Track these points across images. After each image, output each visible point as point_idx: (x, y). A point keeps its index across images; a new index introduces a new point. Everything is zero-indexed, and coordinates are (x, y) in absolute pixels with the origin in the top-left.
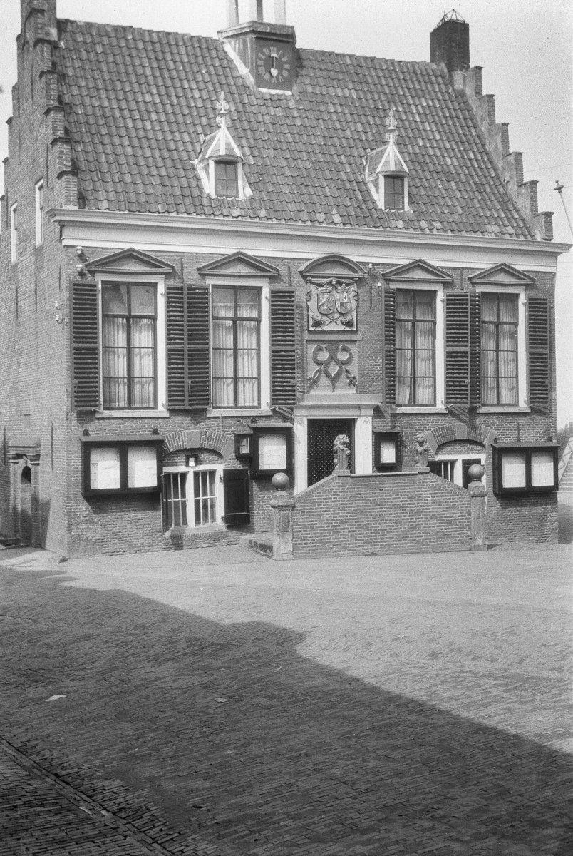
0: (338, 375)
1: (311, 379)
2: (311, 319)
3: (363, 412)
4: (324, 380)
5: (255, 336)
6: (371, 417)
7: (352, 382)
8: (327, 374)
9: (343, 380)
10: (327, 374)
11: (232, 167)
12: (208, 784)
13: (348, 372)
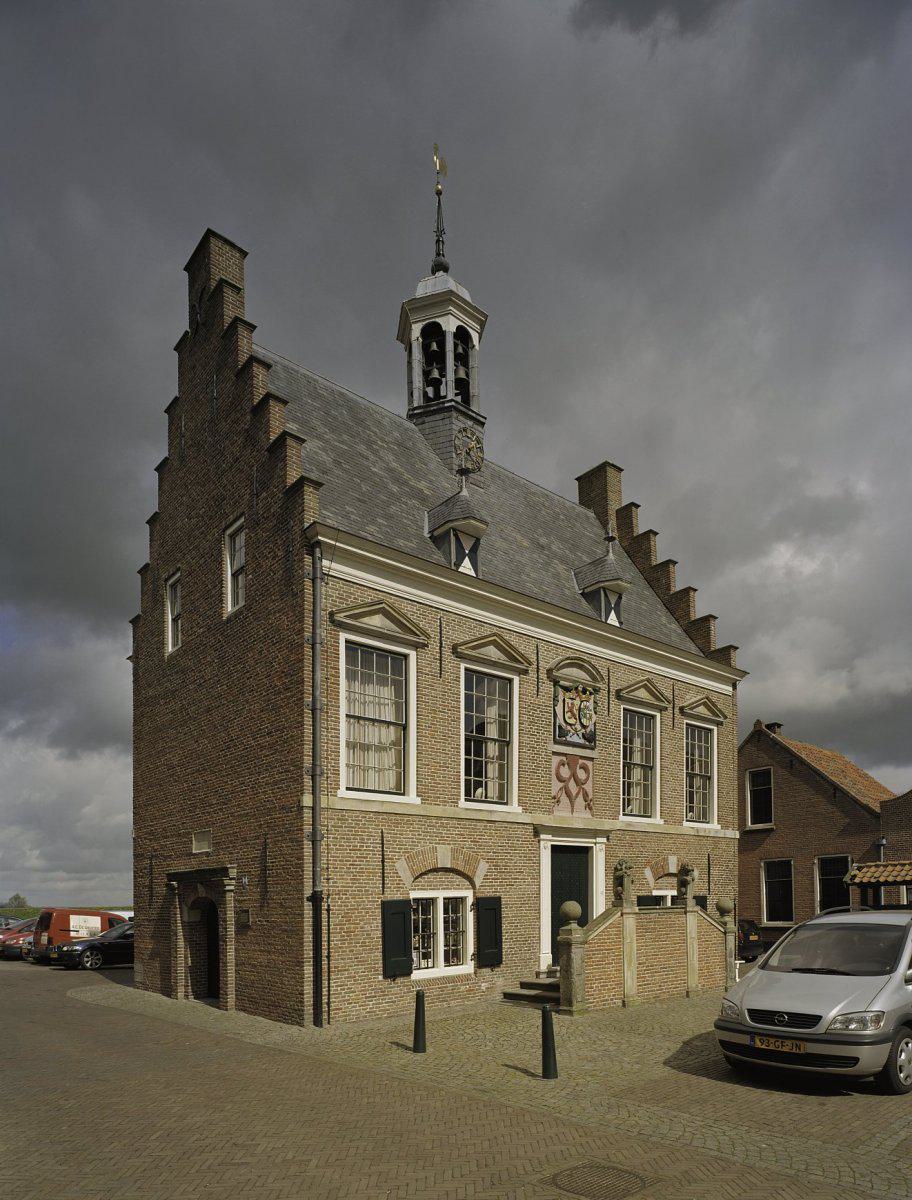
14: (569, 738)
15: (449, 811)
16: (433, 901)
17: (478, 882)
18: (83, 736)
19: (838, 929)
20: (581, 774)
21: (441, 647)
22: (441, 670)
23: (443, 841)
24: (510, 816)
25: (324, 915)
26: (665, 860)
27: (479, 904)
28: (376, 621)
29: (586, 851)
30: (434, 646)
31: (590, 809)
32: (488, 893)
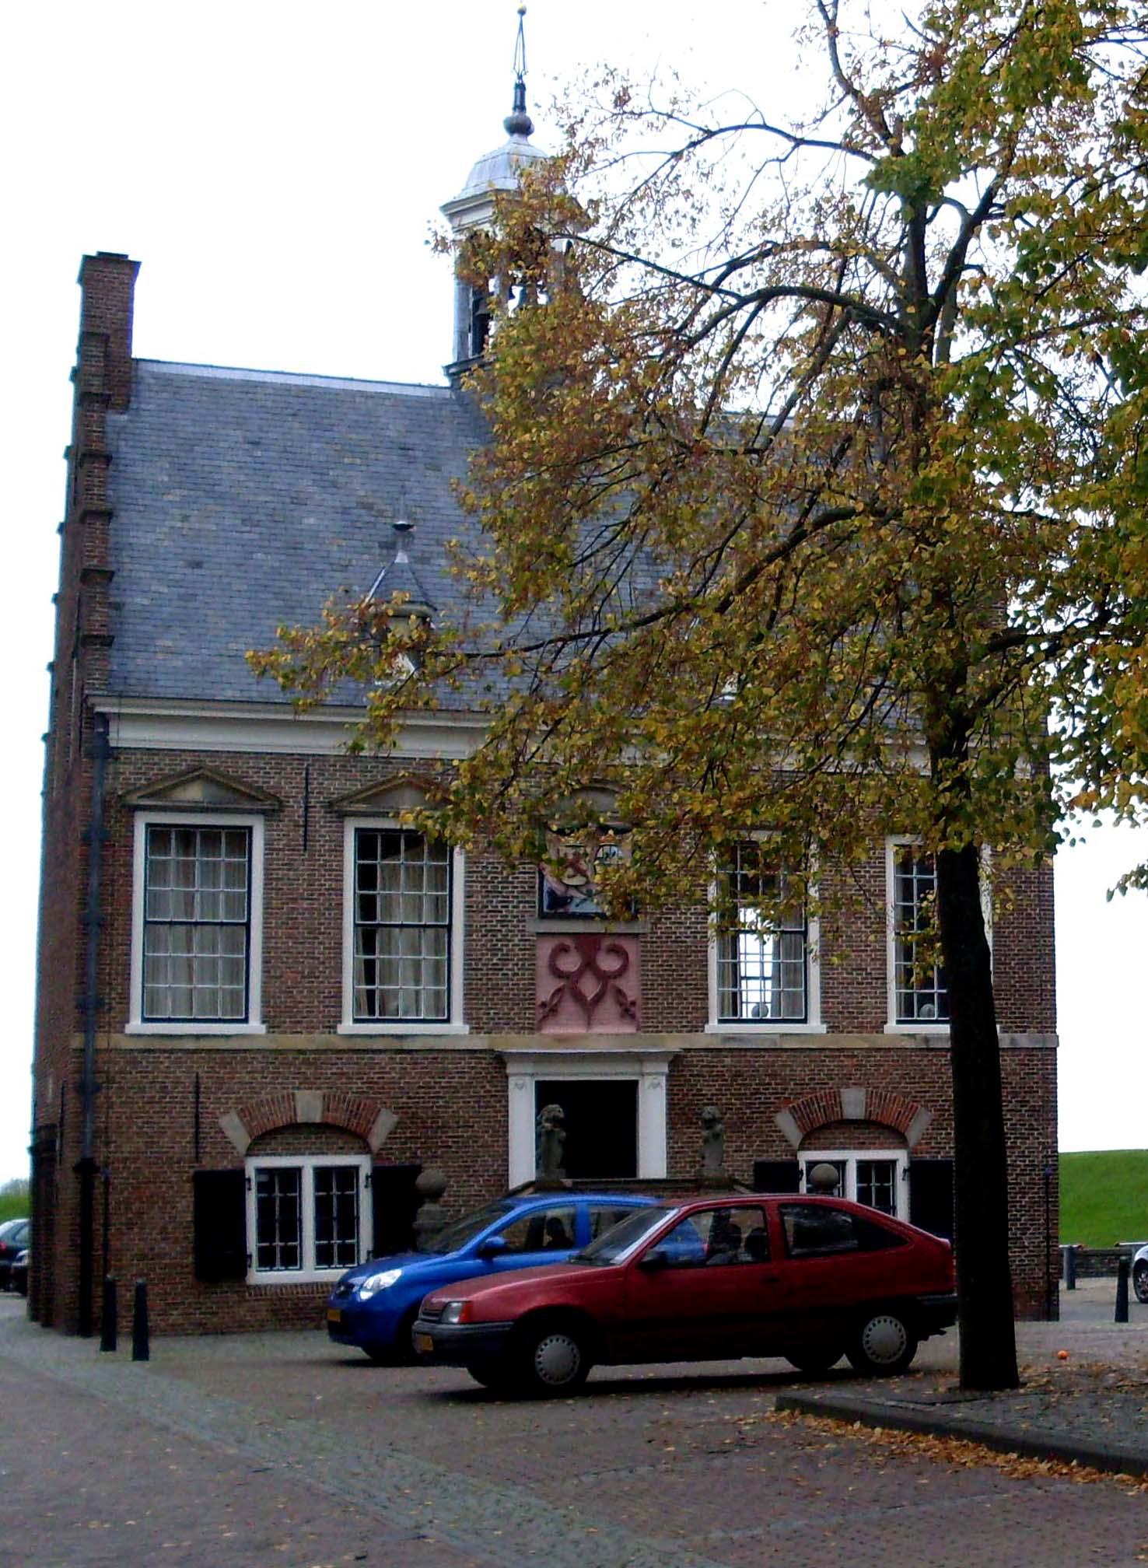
0: (599, 998)
1: (544, 1005)
2: (545, 895)
3: (649, 1068)
4: (569, 1006)
5: (838, 140)
6: (664, 1078)
7: (627, 1011)
8: (579, 997)
9: (609, 1006)
10: (579, 997)
11: (258, 1132)
12: (350, 436)
13: (619, 992)
14: (572, 909)
15: (319, 1039)
16: (297, 1172)
17: (912, 1142)
18: (1014, 1050)
19: (666, 1234)
20: (608, 963)
21: (307, 808)
22: (305, 840)
23: (308, 1084)
24: (443, 1040)
25: (99, 1190)
26: (836, 1096)
27: (378, 1178)
28: (194, 793)
29: (631, 1088)
30: (296, 809)
31: (633, 1017)
32: (397, 1160)
